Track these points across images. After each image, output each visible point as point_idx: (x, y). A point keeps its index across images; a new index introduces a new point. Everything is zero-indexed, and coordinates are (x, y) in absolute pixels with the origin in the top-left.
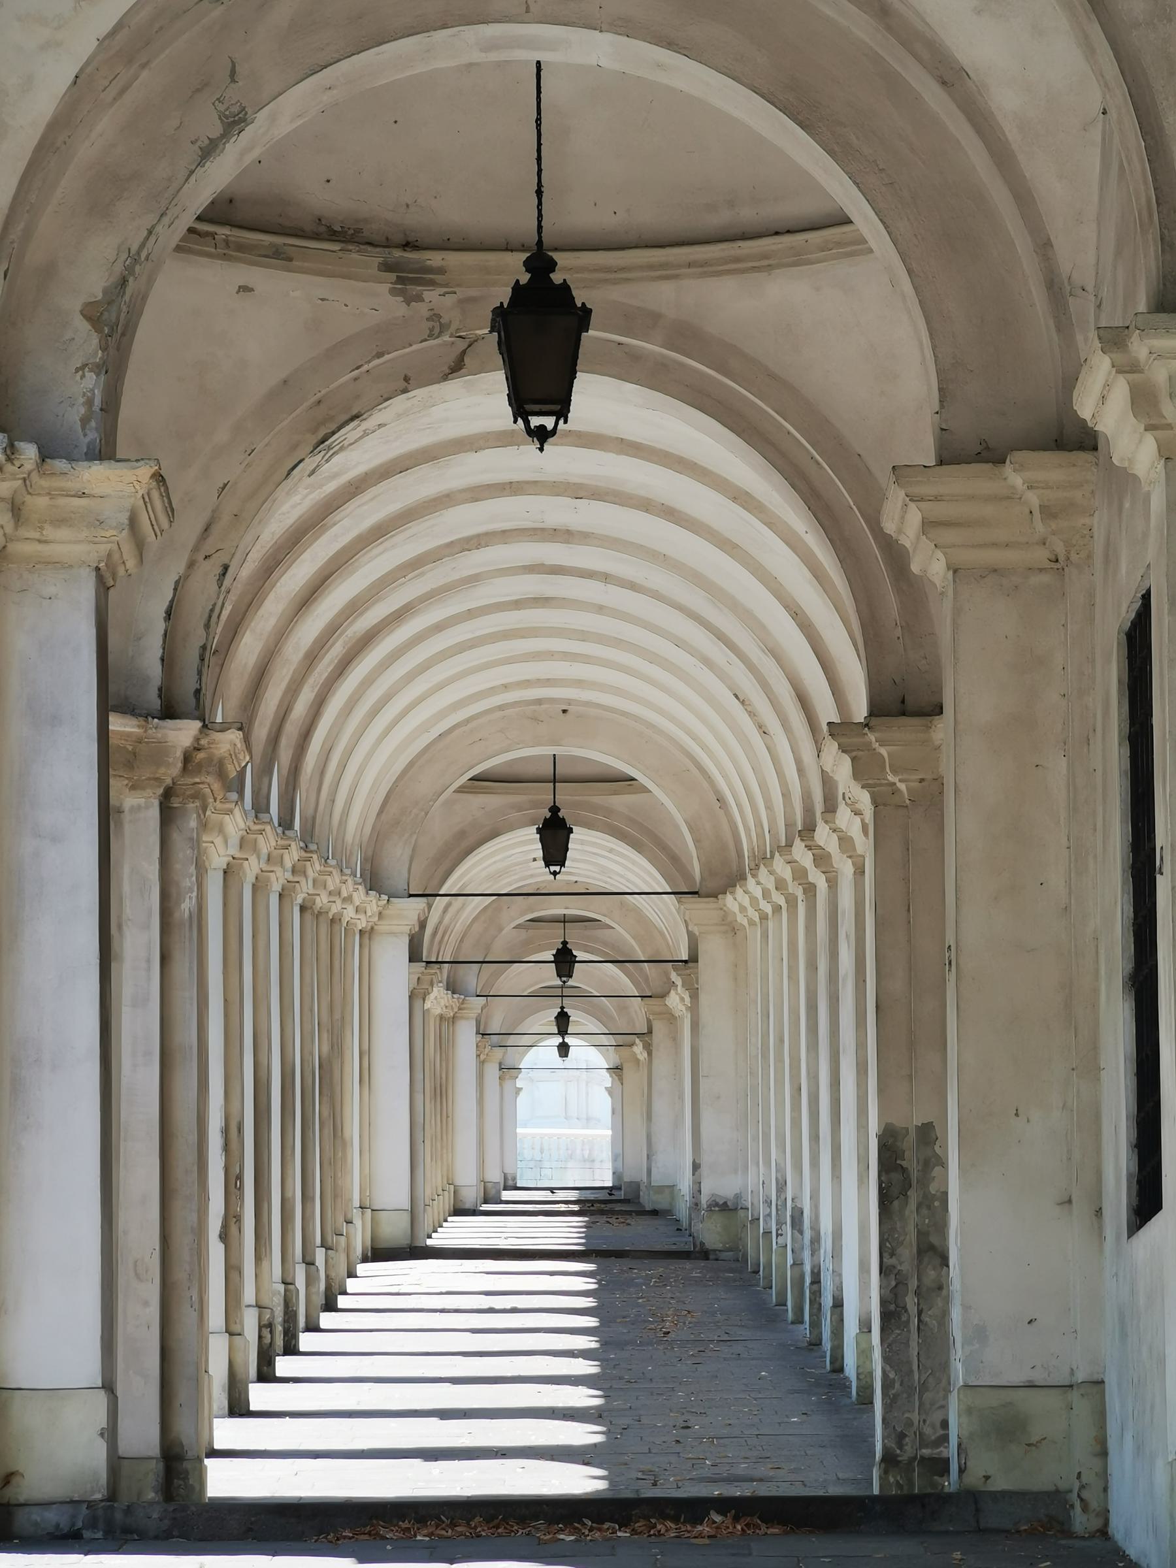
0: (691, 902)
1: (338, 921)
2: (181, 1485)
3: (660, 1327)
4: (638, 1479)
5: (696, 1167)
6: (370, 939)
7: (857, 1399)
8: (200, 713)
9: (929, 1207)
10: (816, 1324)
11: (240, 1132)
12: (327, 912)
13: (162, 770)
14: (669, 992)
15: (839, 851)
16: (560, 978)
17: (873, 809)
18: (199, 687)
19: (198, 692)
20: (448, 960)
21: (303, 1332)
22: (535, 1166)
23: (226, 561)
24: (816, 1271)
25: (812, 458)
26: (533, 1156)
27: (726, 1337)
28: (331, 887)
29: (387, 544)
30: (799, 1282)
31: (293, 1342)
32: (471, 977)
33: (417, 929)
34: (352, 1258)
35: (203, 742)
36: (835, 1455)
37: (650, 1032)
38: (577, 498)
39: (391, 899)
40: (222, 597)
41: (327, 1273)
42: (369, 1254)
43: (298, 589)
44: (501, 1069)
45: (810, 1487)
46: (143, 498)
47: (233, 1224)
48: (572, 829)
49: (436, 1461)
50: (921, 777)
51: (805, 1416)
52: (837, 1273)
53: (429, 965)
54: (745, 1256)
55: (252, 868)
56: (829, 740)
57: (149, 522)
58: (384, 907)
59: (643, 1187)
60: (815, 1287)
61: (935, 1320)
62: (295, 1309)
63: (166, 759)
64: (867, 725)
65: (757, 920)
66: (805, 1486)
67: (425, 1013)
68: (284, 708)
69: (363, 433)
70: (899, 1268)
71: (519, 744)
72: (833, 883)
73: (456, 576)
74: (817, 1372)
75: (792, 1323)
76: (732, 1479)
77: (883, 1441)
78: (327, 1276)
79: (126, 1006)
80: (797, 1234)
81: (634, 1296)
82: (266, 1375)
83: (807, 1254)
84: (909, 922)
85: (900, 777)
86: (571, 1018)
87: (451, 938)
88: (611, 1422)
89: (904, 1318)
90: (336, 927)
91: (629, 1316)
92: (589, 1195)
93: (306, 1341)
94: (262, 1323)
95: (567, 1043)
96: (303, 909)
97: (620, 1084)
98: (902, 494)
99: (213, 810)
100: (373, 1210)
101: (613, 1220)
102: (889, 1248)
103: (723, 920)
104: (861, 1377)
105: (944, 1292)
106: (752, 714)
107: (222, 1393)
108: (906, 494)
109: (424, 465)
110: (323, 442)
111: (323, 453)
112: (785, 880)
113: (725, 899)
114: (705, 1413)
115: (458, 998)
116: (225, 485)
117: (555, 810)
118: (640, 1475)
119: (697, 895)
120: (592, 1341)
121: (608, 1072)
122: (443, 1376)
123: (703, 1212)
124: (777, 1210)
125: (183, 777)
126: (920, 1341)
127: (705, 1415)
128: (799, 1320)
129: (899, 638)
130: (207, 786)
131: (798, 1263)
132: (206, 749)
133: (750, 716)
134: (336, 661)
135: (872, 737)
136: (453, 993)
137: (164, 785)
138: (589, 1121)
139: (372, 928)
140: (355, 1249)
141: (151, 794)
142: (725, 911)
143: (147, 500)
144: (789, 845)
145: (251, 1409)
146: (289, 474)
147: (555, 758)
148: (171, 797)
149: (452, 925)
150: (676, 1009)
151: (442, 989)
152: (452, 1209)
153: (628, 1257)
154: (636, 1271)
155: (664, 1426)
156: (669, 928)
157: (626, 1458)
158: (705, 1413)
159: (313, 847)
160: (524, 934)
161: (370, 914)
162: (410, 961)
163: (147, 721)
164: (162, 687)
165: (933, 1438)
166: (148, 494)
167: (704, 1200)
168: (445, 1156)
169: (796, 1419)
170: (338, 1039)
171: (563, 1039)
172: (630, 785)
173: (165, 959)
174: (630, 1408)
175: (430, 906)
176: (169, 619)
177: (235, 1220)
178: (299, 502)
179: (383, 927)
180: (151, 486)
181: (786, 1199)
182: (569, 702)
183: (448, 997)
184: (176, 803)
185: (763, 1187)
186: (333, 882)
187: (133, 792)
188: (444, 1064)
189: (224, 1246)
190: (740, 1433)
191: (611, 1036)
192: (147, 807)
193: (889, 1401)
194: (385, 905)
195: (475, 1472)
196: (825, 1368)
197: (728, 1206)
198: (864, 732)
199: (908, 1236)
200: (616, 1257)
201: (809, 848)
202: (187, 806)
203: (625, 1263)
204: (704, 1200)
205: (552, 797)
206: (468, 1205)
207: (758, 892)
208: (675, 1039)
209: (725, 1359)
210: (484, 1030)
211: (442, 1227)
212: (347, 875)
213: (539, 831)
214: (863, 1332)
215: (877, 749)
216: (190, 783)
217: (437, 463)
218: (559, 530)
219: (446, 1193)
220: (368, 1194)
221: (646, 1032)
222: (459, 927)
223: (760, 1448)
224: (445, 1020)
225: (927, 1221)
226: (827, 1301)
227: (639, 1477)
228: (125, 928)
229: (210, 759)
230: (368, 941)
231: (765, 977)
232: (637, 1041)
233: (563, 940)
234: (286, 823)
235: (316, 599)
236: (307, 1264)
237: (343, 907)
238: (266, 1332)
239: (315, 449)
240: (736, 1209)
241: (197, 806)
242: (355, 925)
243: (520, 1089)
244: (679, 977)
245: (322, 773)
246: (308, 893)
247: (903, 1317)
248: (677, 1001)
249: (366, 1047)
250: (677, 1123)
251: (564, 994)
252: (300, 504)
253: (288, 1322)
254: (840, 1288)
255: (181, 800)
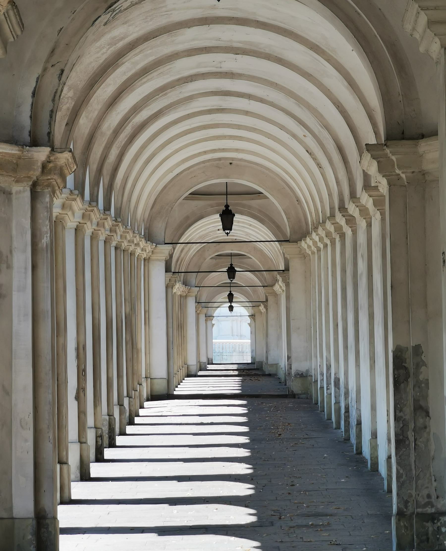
0: (286, 245)
1: (133, 254)
2: (45, 531)
3: (277, 431)
4: (272, 515)
5: (289, 358)
6: (148, 262)
7: (371, 469)
8: (50, 143)
9: (419, 387)
10: (347, 430)
11: (84, 350)
12: (128, 250)
13: (32, 172)
14: (275, 284)
15: (360, 216)
16: (230, 279)
17: (388, 187)
18: (49, 131)
19: (49, 134)
20: (184, 271)
21: (119, 436)
22: (220, 355)
23: (62, 67)
24: (347, 407)
25: (356, 11)
26: (219, 351)
27: (306, 436)
28: (128, 238)
29: (149, 77)
30: (338, 411)
31: (113, 442)
32: (192, 278)
33: (168, 258)
34: (142, 400)
35: (52, 158)
36: (365, 500)
37: (267, 300)
38: (236, 54)
39: (157, 245)
40: (61, 86)
41: (130, 408)
42: (150, 398)
43: (107, 98)
44: (206, 316)
45: (355, 519)
46: (4, 14)
47: (82, 392)
48: (235, 214)
49: (175, 506)
50: (412, 171)
51: (347, 478)
52: (359, 410)
53: (174, 273)
54: (311, 396)
55: (89, 230)
56: (366, 153)
57: (9, 30)
58: (154, 249)
59: (264, 364)
60: (347, 414)
61: (423, 444)
62: (114, 427)
63: (33, 167)
64: (385, 145)
65: (316, 251)
66: (353, 518)
67: (173, 295)
68: (104, 155)
69: (130, 3)
70: (404, 417)
71: (211, 178)
72: (354, 232)
73: (182, 96)
74: (349, 454)
75: (335, 429)
76: (317, 515)
77: (397, 505)
78: (130, 410)
79: (14, 291)
80: (337, 390)
81: (264, 416)
82: (100, 458)
83: (342, 399)
84: (407, 244)
85: (402, 171)
86: (234, 296)
87: (184, 263)
88: (257, 483)
89: (407, 443)
90: (133, 257)
91: (262, 426)
92: (242, 367)
93: (120, 440)
94: (97, 435)
95: (232, 306)
96: (116, 248)
97: (254, 322)
98: (416, 6)
99: (67, 199)
100: (151, 379)
101: (252, 379)
102: (399, 408)
103: (300, 252)
104: (373, 459)
105: (428, 430)
106: (315, 159)
107: (77, 470)
108: (419, 6)
109: (165, 35)
110: (110, 7)
111: (110, 13)
112: (331, 232)
113: (301, 243)
114: (301, 477)
115: (188, 288)
116: (61, 29)
117: (227, 206)
118: (272, 513)
119: (289, 242)
120: (247, 439)
121: (249, 317)
122: (180, 458)
123: (293, 377)
124: (327, 378)
125: (42, 176)
126: (416, 455)
127: (301, 478)
128: (338, 427)
129: (400, 101)
130: (54, 181)
131: (337, 402)
132: (53, 162)
133: (313, 160)
134: (128, 136)
135: (388, 151)
136: (186, 286)
137: (32, 180)
138: (241, 337)
139: (149, 258)
140: (143, 396)
141: (26, 185)
142: (301, 248)
143: (7, 16)
144: (324, 222)
145: (91, 476)
146: (93, 23)
147: (227, 184)
148: (37, 186)
149: (185, 258)
150: (278, 291)
151: (181, 284)
152: (186, 374)
153: (261, 397)
154: (264, 404)
155: (282, 485)
156: (274, 257)
157: (265, 503)
158: (301, 477)
159: (119, 220)
160: (214, 261)
161: (148, 252)
162: (166, 272)
163: (23, 148)
164: (31, 131)
165: (423, 503)
166: (7, 13)
167: (293, 372)
168: (183, 353)
169: (343, 480)
170: (134, 305)
171: (231, 304)
172: (259, 196)
173: (34, 267)
174: (266, 475)
175: (174, 249)
176: (34, 97)
177: (82, 390)
178: (105, 52)
179: (154, 257)
180: (8, 8)
181: (331, 373)
182: (233, 159)
183: (183, 288)
184: (39, 189)
185: (320, 368)
186: (130, 236)
187: (17, 184)
188: (182, 315)
189: (77, 402)
190: (318, 488)
191: (250, 302)
192: (24, 191)
193: (400, 485)
194: (155, 248)
195: (194, 512)
196: (353, 452)
197: (303, 375)
198: (384, 148)
199: (408, 402)
200: (255, 398)
201: (343, 216)
202: (44, 190)
203: (260, 400)
204: (293, 372)
205: (226, 201)
206: (193, 373)
207: (317, 239)
208: (277, 303)
209: (307, 448)
210: (199, 301)
211: (182, 382)
212: (136, 234)
213: (220, 215)
214: (373, 438)
215: (391, 157)
216: (46, 179)
217: (171, 34)
218: (229, 73)
219: (184, 368)
220: (149, 372)
221: (265, 301)
222: (187, 259)
223: (329, 497)
224: (183, 297)
225: (418, 394)
226: (353, 422)
227: (272, 514)
228: (13, 252)
229: (55, 167)
230: (147, 264)
231: (319, 276)
232: (262, 304)
233: (231, 263)
234: (107, 208)
235: (116, 103)
236: (120, 405)
237: (135, 248)
238: (99, 439)
239: (106, 10)
240: (307, 376)
241: (49, 191)
242: (142, 256)
243: (214, 324)
244: (280, 277)
245: (124, 188)
246: (118, 241)
247: (406, 442)
248: (279, 287)
249: (147, 309)
250: (279, 337)
251: (231, 286)
252: (106, 53)
253: (111, 433)
254: (360, 416)
255: (41, 188)
